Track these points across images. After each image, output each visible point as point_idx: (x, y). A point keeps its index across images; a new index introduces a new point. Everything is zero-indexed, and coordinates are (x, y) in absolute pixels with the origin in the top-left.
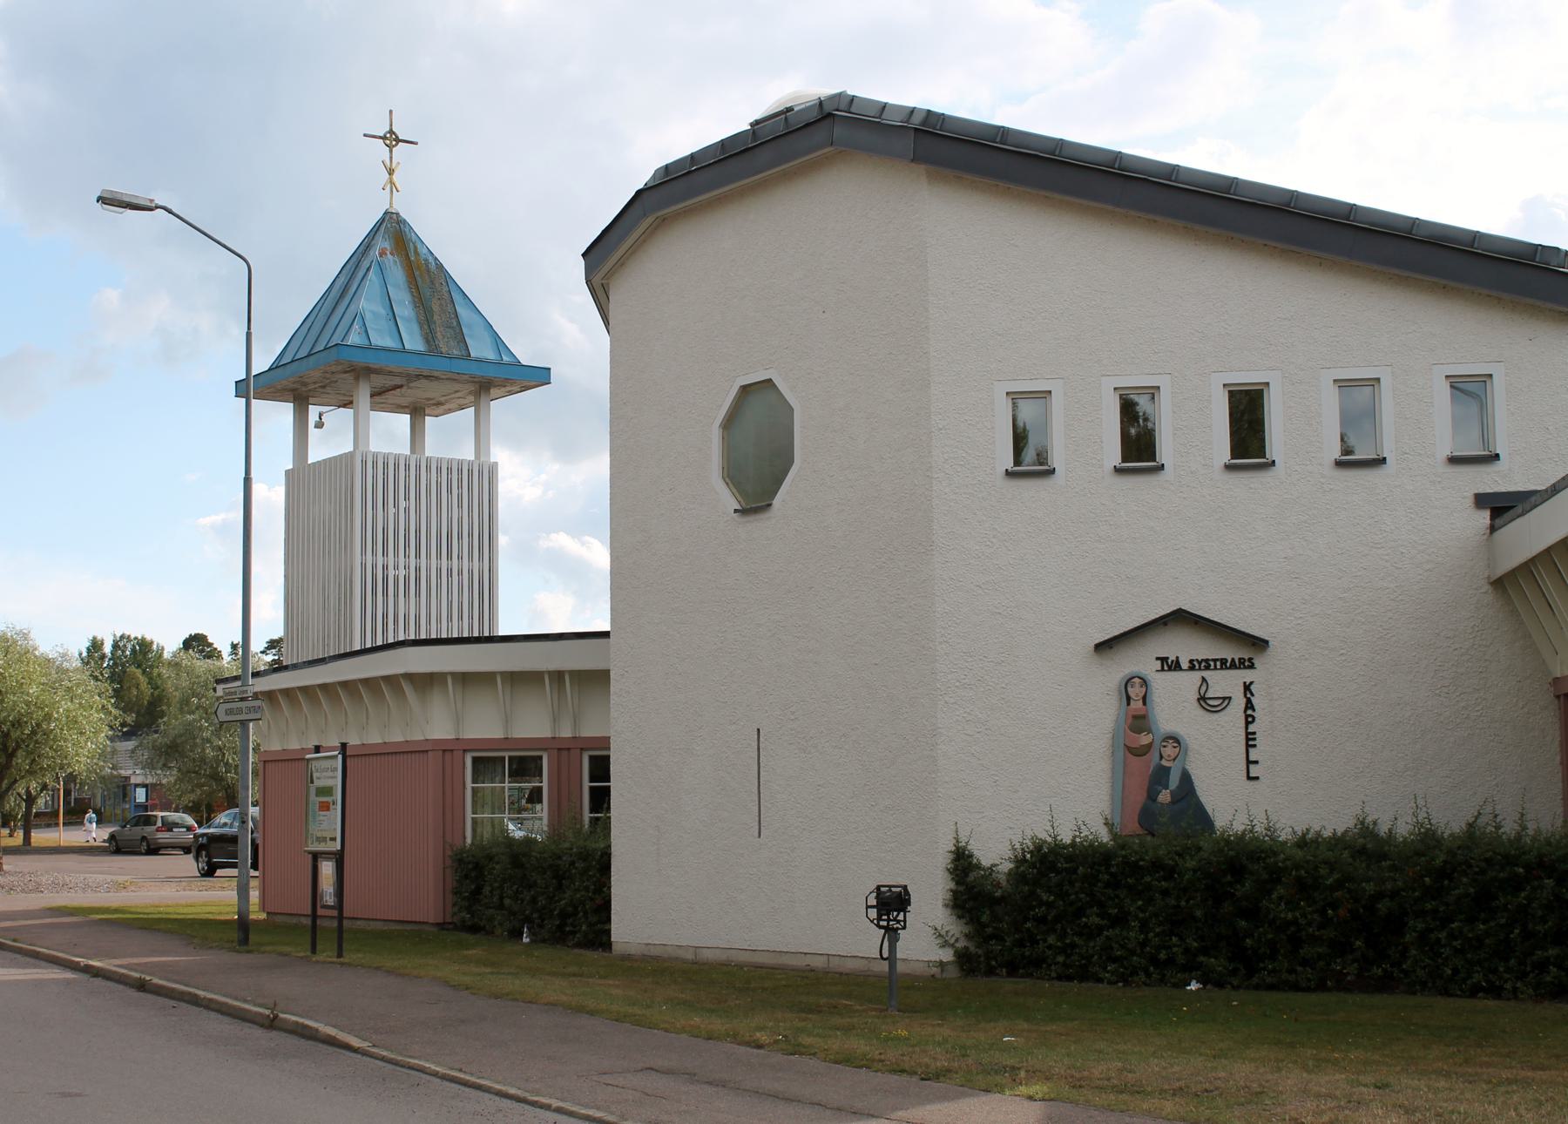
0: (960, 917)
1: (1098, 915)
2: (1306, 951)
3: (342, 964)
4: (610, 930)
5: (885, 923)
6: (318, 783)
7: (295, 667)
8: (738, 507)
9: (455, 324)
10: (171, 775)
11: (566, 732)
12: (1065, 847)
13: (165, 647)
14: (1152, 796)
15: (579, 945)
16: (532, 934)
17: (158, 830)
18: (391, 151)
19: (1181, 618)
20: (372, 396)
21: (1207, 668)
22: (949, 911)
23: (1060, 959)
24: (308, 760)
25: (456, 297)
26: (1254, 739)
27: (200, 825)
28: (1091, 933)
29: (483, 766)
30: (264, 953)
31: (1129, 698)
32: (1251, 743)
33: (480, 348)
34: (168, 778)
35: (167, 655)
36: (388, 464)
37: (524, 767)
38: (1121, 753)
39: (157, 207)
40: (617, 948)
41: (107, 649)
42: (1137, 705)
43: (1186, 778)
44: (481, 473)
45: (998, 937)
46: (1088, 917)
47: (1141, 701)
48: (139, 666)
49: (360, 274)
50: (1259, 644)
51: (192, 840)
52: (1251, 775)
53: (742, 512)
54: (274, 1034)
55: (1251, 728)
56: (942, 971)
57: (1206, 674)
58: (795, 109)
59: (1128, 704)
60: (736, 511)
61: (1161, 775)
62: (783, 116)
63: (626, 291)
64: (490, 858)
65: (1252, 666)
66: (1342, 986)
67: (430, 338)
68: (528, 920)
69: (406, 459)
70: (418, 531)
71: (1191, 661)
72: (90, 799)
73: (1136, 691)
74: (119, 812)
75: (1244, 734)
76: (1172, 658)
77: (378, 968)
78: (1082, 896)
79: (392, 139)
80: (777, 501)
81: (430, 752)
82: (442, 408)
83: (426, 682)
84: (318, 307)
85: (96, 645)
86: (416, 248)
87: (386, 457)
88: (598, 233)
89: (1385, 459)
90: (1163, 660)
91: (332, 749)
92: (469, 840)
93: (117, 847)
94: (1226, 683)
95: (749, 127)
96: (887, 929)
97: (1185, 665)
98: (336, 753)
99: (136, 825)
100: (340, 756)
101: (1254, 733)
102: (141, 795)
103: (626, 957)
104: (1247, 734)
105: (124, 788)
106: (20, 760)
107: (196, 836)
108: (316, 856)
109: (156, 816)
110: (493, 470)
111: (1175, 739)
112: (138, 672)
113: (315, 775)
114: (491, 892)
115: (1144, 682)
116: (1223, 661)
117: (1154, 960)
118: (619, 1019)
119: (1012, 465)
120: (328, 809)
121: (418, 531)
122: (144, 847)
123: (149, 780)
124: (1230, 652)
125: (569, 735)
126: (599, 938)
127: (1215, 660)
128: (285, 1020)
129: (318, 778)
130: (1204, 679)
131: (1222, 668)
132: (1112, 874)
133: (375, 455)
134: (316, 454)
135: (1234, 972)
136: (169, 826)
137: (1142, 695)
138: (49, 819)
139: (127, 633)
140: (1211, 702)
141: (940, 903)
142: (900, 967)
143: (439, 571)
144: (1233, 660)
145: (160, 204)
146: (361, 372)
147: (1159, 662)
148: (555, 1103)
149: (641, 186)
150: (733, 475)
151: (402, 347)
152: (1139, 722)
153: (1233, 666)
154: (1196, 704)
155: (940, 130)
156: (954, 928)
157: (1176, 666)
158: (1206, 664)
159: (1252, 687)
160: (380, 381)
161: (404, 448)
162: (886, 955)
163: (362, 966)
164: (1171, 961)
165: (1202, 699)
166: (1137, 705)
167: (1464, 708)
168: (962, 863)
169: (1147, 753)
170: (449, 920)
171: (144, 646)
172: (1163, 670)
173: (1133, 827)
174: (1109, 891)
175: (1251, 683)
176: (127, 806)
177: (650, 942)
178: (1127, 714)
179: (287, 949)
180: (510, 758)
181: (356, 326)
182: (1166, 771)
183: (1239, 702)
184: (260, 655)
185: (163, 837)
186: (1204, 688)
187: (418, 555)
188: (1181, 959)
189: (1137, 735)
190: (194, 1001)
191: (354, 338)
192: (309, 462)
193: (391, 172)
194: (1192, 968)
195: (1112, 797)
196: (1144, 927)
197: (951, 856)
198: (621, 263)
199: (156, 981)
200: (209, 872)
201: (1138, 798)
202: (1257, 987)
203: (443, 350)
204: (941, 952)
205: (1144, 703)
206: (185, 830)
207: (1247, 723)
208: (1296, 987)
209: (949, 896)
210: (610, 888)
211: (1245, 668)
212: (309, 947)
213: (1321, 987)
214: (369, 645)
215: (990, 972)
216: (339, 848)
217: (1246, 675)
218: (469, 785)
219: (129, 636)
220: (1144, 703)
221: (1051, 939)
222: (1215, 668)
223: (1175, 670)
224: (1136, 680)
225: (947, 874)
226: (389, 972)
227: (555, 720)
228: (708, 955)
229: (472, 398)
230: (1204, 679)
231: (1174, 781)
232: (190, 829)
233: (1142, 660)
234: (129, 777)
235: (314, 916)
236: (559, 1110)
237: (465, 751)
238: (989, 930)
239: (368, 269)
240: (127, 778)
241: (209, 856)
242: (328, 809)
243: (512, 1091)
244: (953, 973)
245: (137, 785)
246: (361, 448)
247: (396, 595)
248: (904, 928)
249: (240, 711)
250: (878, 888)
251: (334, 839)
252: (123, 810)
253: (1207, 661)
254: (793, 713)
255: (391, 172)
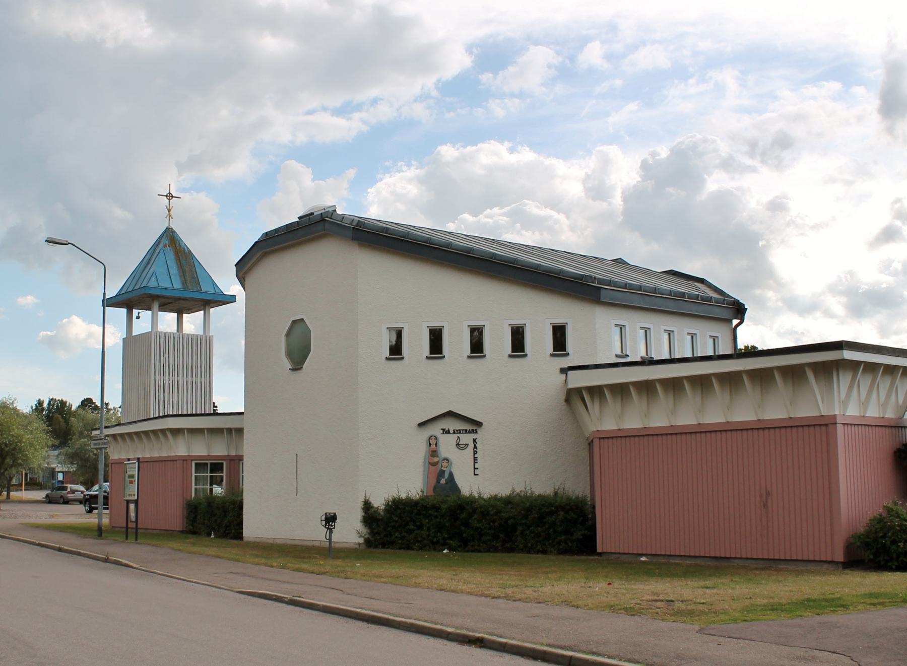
0: (366, 526)
1: (413, 525)
2: (484, 538)
3: (137, 543)
4: (242, 532)
5: (327, 526)
6: (129, 473)
7: (124, 424)
8: (291, 368)
9: (195, 276)
10: (74, 467)
11: (233, 453)
12: (402, 500)
13: (73, 405)
14: (438, 481)
15: (232, 538)
16: (215, 534)
17: (68, 493)
18: (169, 202)
19: (450, 414)
20: (159, 307)
21: (460, 433)
22: (362, 524)
23: (400, 542)
24: (126, 464)
25: (196, 264)
26: (477, 460)
27: (87, 490)
28: (410, 532)
29: (200, 467)
30: (108, 539)
31: (430, 444)
32: (476, 461)
33: (205, 287)
34: (73, 468)
35: (73, 408)
36: (166, 336)
37: (216, 467)
38: (427, 464)
39: (69, 244)
40: (245, 539)
41: (45, 405)
42: (433, 446)
43: (451, 475)
44: (206, 340)
45: (378, 533)
46: (409, 526)
47: (435, 446)
48: (60, 414)
49: (155, 255)
50: (479, 424)
51: (82, 498)
52: (476, 473)
53: (293, 370)
54: (107, 564)
55: (476, 456)
56: (359, 546)
57: (459, 435)
58: (315, 214)
59: (430, 446)
60: (290, 369)
61: (442, 473)
62: (308, 218)
63: (250, 280)
64: (200, 504)
65: (476, 432)
66: (496, 550)
67: (185, 283)
68: (213, 529)
69: (175, 333)
70: (178, 366)
71: (454, 430)
72: (36, 478)
73: (433, 441)
74: (50, 484)
75: (473, 458)
76: (447, 429)
77: (149, 544)
78: (407, 518)
79: (170, 196)
80: (304, 366)
81: (178, 461)
82: (190, 311)
83: (176, 432)
84: (137, 270)
85: (40, 403)
86: (179, 244)
87: (165, 333)
88: (241, 257)
89: (527, 354)
90: (444, 430)
91: (134, 459)
92: (193, 495)
93: (50, 500)
94: (466, 439)
95: (298, 220)
96: (328, 528)
97: (451, 432)
98: (135, 461)
99: (58, 490)
100: (137, 463)
101: (477, 458)
102: (60, 477)
103: (248, 542)
104: (474, 458)
105: (53, 473)
106: (9, 461)
107: (85, 495)
108: (128, 502)
109: (67, 487)
110: (211, 338)
111: (447, 460)
112: (60, 416)
113: (128, 470)
114: (200, 518)
115: (436, 438)
116: (466, 430)
117: (433, 543)
118: (229, 559)
119: (389, 355)
120: (132, 483)
121: (178, 366)
122: (62, 500)
123: (65, 469)
124: (469, 427)
125: (234, 454)
126: (239, 536)
127: (463, 430)
128: (111, 559)
129: (129, 471)
130: (458, 437)
131: (465, 433)
132: (418, 510)
133: (161, 333)
134: (135, 332)
135: (460, 546)
136: (73, 492)
137: (435, 443)
138: (18, 487)
139: (54, 398)
140: (461, 446)
141: (359, 521)
142: (333, 544)
143: (187, 382)
144: (469, 430)
145: (70, 242)
146: (154, 297)
147: (442, 431)
148: (194, 580)
149: (257, 240)
150: (290, 355)
151: (172, 287)
152: (434, 453)
153: (470, 432)
154: (456, 446)
155: (363, 228)
156: (364, 530)
157: (448, 432)
158: (459, 432)
159: (477, 441)
160: (163, 301)
161: (173, 329)
162: (328, 538)
163: (144, 544)
164: (438, 542)
165: (458, 445)
166: (433, 446)
167: (555, 449)
168: (367, 506)
169: (436, 465)
170: (185, 529)
171: (63, 403)
172: (443, 433)
173: (431, 493)
174: (417, 517)
175: (476, 439)
176: (54, 482)
177: (257, 536)
178: (429, 450)
179: (117, 538)
180: (210, 463)
181: (153, 278)
182: (444, 471)
183: (471, 446)
184: (118, 409)
185: (71, 496)
186: (458, 440)
187: (178, 375)
188: (441, 541)
189: (432, 458)
190: (79, 554)
191: (153, 283)
192: (133, 335)
193: (169, 210)
194: (444, 545)
195: (424, 481)
196: (429, 529)
197: (363, 503)
198: (250, 269)
199: (65, 548)
200: (90, 511)
201: (433, 482)
202: (468, 551)
203: (190, 288)
204: (359, 539)
205: (436, 446)
206: (80, 493)
207: (474, 454)
208: (479, 551)
209: (362, 518)
210: (243, 515)
211: (474, 433)
212: (125, 536)
213: (488, 551)
214: (157, 416)
215: (376, 547)
216: (136, 498)
217: (474, 436)
218: (194, 474)
219: (55, 399)
220: (436, 446)
221: (397, 534)
222: (463, 433)
223: (448, 433)
224: (433, 437)
225: (362, 510)
226: (153, 545)
227: (228, 448)
228: (279, 542)
229: (202, 307)
230: (458, 437)
231: (447, 475)
232: (82, 492)
233: (435, 430)
234: (55, 468)
235: (127, 527)
236: (195, 582)
237: (192, 460)
238: (375, 531)
239: (159, 253)
240: (54, 469)
241: (90, 504)
242: (132, 483)
243: (182, 578)
244: (363, 547)
245: (59, 472)
246: (155, 330)
247: (169, 393)
248: (334, 528)
249: (99, 444)
250: (326, 514)
251: (134, 495)
252: (53, 484)
253: (460, 430)
254: (309, 448)
255: (169, 210)
